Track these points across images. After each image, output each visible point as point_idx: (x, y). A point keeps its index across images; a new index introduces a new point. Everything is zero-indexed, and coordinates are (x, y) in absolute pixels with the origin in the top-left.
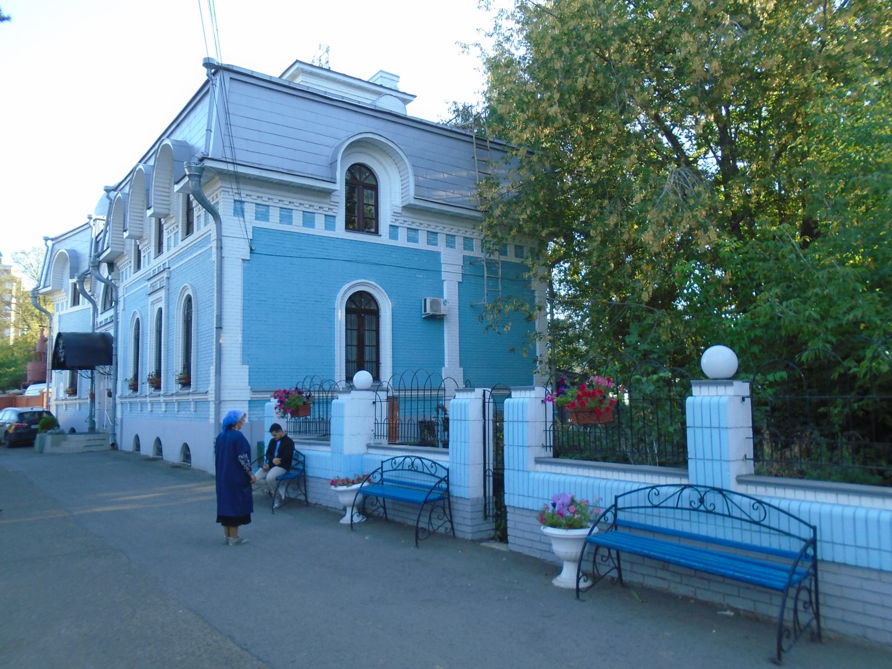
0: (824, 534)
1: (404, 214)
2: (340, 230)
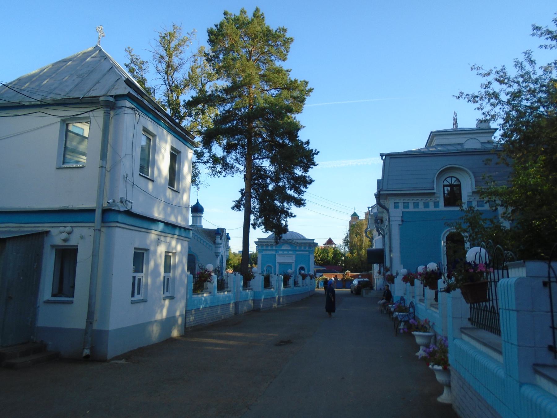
2: (441, 207)
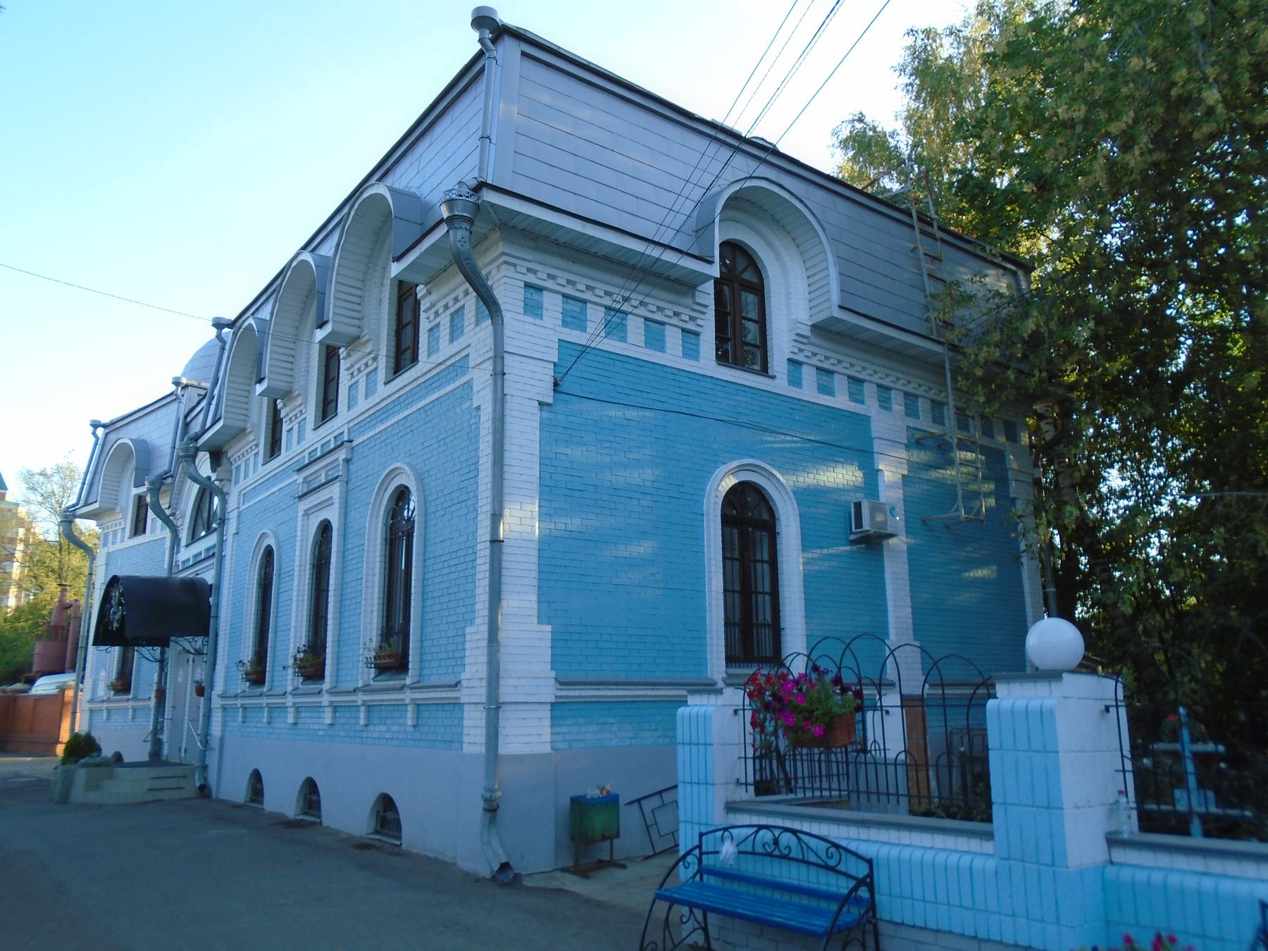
0: (881, 879)
1: (813, 340)
2: (706, 362)
